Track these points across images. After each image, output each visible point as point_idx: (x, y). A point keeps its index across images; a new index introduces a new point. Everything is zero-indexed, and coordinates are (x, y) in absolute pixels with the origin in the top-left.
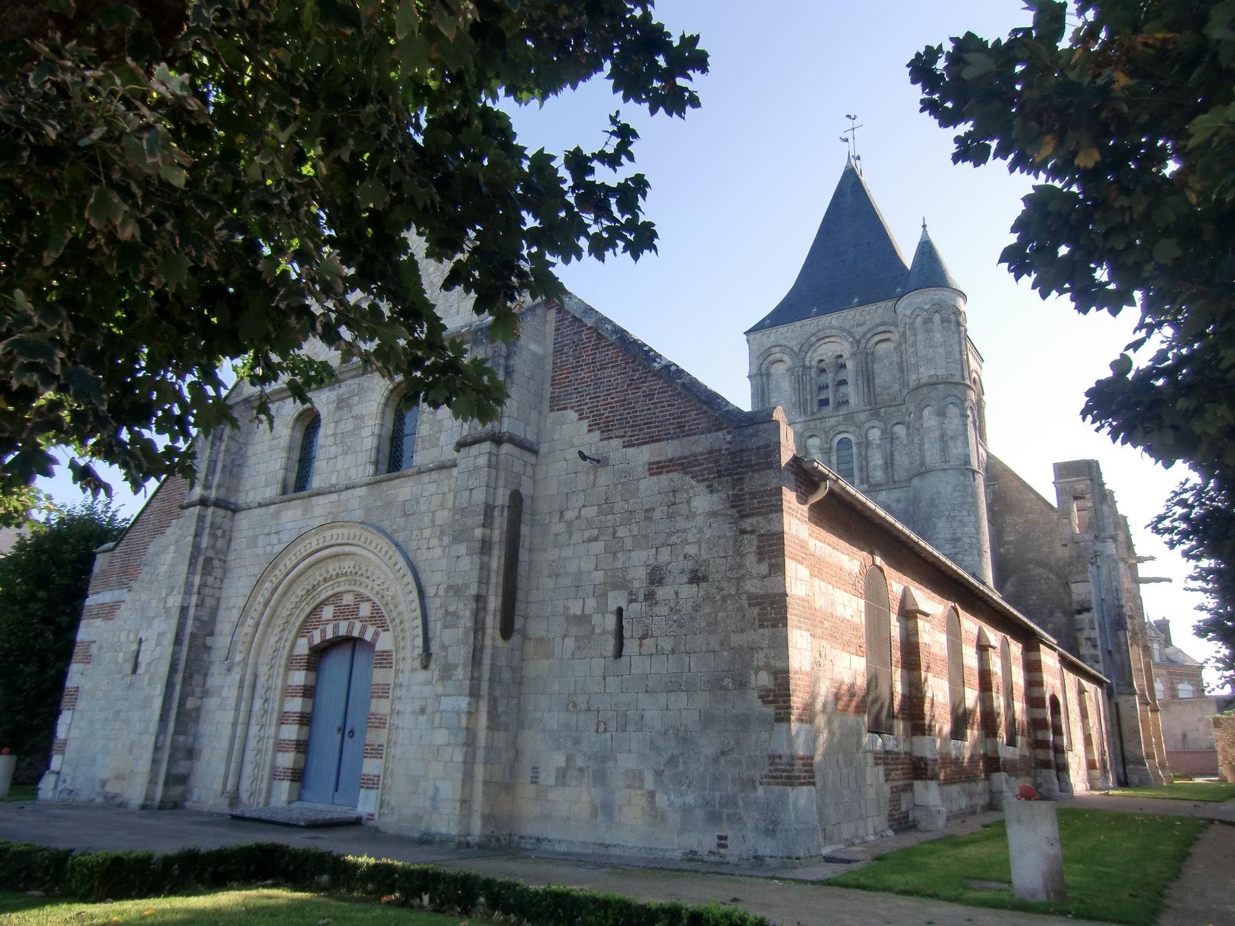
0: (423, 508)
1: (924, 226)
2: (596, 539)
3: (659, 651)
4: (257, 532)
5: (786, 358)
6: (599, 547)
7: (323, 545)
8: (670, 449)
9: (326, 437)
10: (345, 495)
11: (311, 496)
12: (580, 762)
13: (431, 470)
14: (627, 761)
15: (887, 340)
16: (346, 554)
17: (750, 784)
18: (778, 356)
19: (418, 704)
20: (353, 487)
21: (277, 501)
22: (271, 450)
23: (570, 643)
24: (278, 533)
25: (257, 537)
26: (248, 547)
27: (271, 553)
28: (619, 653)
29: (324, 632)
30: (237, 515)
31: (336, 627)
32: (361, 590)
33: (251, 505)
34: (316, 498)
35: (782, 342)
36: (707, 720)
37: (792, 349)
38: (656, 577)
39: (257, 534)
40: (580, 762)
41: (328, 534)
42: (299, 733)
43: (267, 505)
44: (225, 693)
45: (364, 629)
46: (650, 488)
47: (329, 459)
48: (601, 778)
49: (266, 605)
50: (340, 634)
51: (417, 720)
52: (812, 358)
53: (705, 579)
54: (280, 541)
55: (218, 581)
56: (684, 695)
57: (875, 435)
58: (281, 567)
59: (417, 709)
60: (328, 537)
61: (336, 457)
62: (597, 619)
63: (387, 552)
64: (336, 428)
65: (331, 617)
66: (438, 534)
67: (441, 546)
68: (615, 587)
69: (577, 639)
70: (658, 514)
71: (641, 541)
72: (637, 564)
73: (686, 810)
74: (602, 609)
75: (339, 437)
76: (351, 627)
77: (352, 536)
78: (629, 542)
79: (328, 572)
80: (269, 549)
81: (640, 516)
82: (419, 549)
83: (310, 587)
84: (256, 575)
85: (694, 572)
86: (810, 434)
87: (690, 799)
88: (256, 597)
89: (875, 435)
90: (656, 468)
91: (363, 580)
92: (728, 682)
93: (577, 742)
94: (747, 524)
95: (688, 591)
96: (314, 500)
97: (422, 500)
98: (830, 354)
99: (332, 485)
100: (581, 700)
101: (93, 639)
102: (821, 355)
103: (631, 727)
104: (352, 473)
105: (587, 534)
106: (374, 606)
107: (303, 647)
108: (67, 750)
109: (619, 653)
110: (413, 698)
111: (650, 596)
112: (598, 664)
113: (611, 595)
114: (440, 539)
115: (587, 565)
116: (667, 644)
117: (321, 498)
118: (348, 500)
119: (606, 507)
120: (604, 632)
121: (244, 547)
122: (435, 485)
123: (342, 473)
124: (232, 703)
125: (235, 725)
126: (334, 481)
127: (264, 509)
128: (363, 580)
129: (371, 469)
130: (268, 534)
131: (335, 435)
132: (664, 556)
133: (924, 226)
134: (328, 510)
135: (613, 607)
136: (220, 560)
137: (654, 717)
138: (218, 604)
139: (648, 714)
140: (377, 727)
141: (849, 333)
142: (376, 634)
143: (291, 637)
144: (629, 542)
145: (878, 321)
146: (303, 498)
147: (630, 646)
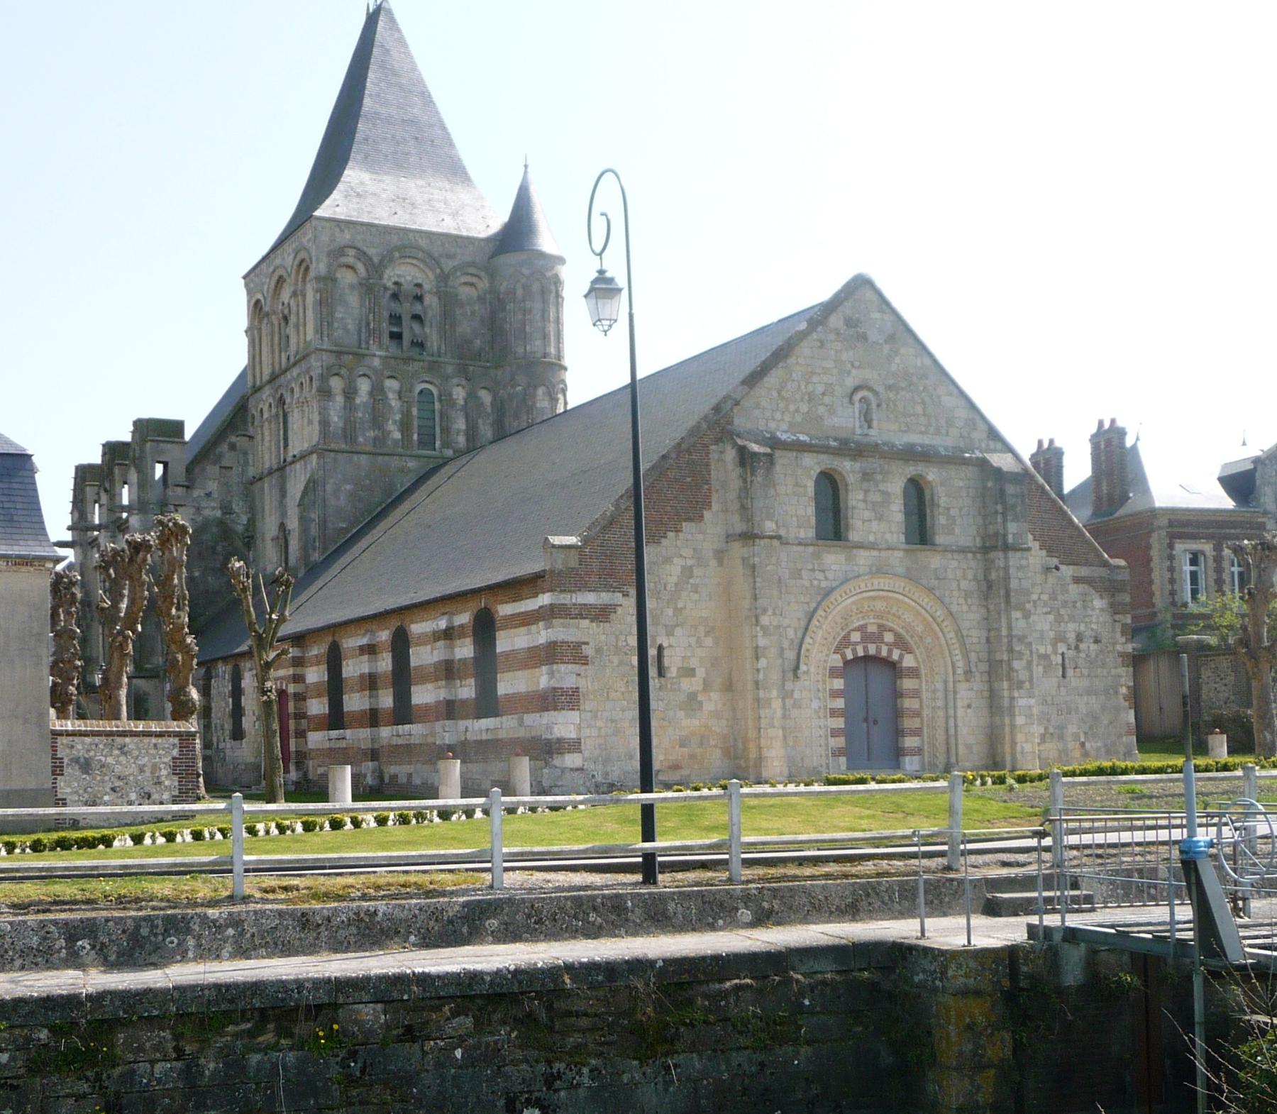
1: (526, 166)
2: (1049, 613)
3: (1082, 676)
5: (360, 267)
6: (1051, 618)
8: (1084, 571)
10: (884, 554)
12: (1051, 730)
13: (953, 551)
14: (1072, 729)
15: (472, 284)
17: (1120, 736)
18: (350, 260)
19: (966, 702)
23: (1041, 669)
28: (1064, 676)
29: (854, 651)
31: (865, 649)
35: (360, 245)
36: (1103, 708)
37: (371, 259)
38: (1079, 638)
40: (1051, 730)
41: (876, 581)
45: (890, 652)
46: (1074, 589)
47: (864, 521)
48: (1061, 737)
52: (390, 276)
53: (1100, 641)
56: (1094, 697)
57: (459, 394)
60: (897, 586)
62: (1053, 657)
68: (1061, 641)
69: (1044, 667)
70: (1078, 605)
71: (1072, 619)
72: (1071, 629)
73: (1098, 749)
74: (1055, 652)
76: (854, 651)
78: (1066, 618)
81: (1070, 605)
85: (1096, 637)
86: (389, 373)
87: (1099, 744)
89: (459, 394)
90: (1077, 580)
92: (1111, 691)
93: (1049, 720)
94: (1117, 617)
95: (1093, 647)
98: (409, 278)
100: (1049, 699)
101: (586, 640)
102: (399, 276)
103: (1073, 713)
104: (888, 536)
105: (1045, 610)
107: (837, 661)
108: (583, 748)
109: (1064, 676)
111: (1077, 648)
112: (1055, 680)
113: (1059, 645)
114: (966, 600)
115: (1047, 627)
116: (1085, 672)
117: (862, 551)
119: (1053, 597)
120: (1057, 664)
126: (871, 538)
129: (902, 538)
132: (1082, 627)
133: (526, 166)
135: (1060, 651)
137: (1083, 709)
139: (1080, 706)
141: (438, 263)
142: (901, 656)
144: (1066, 618)
145: (469, 259)
147: (1070, 672)
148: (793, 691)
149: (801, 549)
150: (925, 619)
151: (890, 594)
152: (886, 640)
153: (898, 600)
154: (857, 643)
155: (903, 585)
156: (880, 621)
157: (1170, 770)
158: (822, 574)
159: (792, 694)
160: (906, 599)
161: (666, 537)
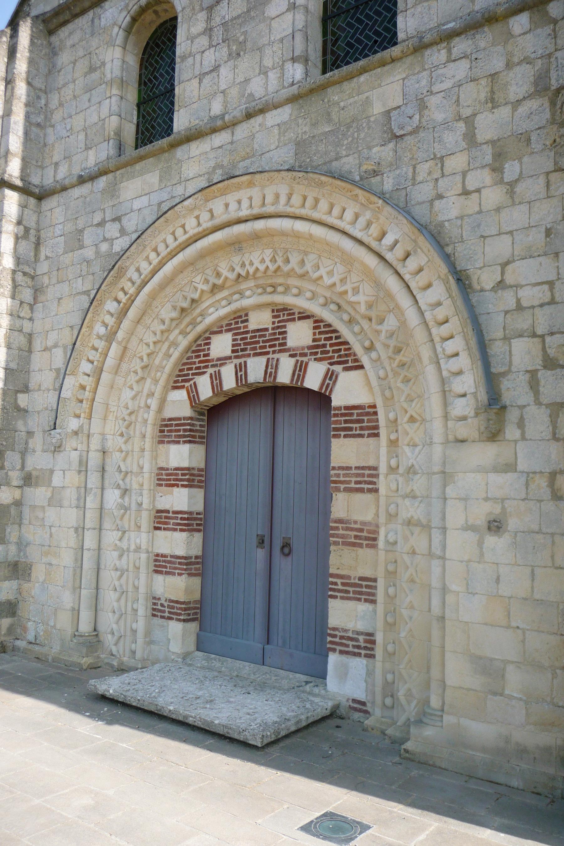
0: (439, 116)
4: (81, 224)
7: (209, 224)
9: (192, 38)
10: (242, 131)
11: (174, 146)
16: (256, 237)
20: (262, 111)
21: (111, 166)
22: (89, 89)
24: (117, 219)
25: (81, 231)
26: (69, 250)
27: (109, 254)
29: (216, 379)
30: (44, 203)
31: (241, 370)
32: (289, 300)
33: (67, 182)
34: (185, 147)
39: (80, 226)
41: (218, 206)
42: (189, 544)
43: (92, 178)
44: (57, 480)
47: (201, 77)
49: (110, 337)
50: (251, 379)
51: (480, 544)
54: (123, 232)
55: (26, 308)
58: (132, 273)
59: (481, 521)
61: (216, 68)
63: (357, 216)
64: (209, 19)
65: (228, 353)
66: (489, 159)
67: (501, 181)
75: (218, 34)
76: (216, 379)
77: (269, 199)
79: (218, 275)
80: (104, 247)
82: (440, 197)
83: (185, 305)
84: (87, 293)
88: (91, 327)
91: (292, 281)
96: (180, 152)
97: (433, 101)
99: (213, 119)
106: (318, 322)
110: (465, 499)
118: (252, 137)
121: (61, 251)
122: (464, 65)
123: (234, 92)
124: (70, 495)
125: (80, 530)
126: (217, 108)
127: (88, 185)
128: (292, 281)
130: (101, 224)
131: (209, 31)
134: (212, 163)
136: (25, 274)
138: (30, 342)
140: (354, 545)
142: (330, 376)
143: (158, 390)
146: (162, 151)
148: (52, 471)
149: (85, 189)
150: (131, 333)
151: (260, 225)
152: (291, 342)
153: (297, 236)
154: (223, 360)
155: (283, 191)
156: (279, 299)
157: (391, 591)
158: (117, 225)
159: (50, 481)
160: (300, 226)
161: (476, 128)
